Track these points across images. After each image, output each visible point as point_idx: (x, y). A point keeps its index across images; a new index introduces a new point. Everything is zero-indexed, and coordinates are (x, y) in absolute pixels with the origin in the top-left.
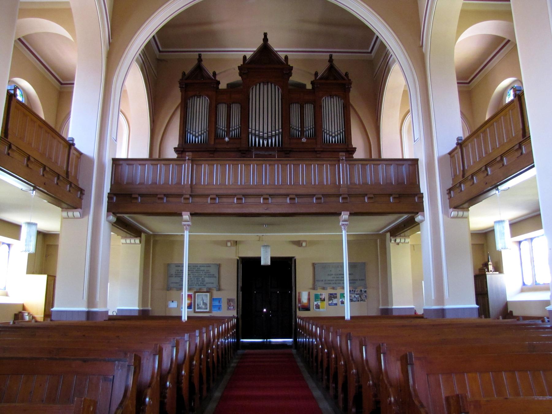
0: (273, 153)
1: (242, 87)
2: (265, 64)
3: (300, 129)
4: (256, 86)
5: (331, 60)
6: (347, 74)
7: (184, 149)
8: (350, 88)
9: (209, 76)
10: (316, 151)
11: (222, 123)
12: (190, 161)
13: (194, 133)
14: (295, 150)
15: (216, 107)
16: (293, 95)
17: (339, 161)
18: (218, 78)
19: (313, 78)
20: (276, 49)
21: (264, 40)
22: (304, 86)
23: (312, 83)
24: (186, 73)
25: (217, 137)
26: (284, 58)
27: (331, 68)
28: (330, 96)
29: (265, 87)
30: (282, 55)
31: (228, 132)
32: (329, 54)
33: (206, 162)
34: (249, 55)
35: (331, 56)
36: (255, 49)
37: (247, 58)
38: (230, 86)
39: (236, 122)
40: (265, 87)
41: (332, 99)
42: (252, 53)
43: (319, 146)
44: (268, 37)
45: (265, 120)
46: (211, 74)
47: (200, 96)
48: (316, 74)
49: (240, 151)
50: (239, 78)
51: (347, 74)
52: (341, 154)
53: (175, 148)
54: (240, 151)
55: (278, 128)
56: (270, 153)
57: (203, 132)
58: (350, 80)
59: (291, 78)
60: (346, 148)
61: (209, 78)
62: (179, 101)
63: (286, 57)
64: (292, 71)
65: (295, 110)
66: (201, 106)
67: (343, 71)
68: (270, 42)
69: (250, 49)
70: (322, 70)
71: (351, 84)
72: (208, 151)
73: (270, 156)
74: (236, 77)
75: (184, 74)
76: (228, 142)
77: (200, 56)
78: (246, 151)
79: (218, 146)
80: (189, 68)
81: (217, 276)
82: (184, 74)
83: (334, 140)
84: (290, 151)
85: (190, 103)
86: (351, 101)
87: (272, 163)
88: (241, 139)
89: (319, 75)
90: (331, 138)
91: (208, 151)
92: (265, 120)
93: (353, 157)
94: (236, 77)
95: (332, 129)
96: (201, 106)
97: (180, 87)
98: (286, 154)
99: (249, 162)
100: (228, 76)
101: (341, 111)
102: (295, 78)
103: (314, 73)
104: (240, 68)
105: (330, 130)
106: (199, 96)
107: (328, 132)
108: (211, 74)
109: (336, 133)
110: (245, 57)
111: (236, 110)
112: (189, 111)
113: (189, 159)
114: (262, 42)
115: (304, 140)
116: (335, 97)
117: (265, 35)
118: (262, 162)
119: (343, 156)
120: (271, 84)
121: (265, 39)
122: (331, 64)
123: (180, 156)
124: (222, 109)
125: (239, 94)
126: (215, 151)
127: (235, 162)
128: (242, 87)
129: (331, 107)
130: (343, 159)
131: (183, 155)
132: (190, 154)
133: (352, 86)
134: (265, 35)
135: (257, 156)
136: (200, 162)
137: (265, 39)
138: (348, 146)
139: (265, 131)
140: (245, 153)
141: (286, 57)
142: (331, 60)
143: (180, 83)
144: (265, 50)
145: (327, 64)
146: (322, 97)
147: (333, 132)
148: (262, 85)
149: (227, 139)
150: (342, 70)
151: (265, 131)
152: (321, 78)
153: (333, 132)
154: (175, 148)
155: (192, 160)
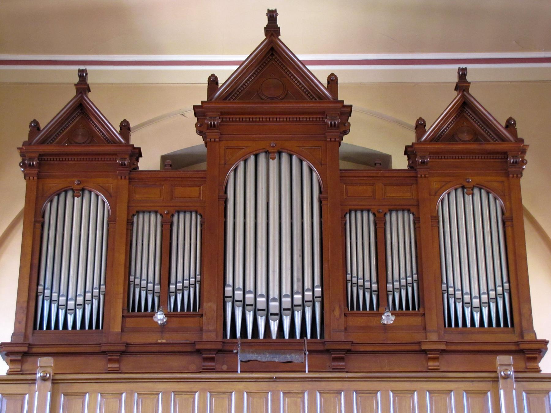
0: (296, 358)
1: (203, 166)
2: (271, 100)
3: (375, 287)
4: (245, 161)
5: (462, 84)
6: (510, 125)
7: (30, 346)
8: (524, 162)
9: (108, 131)
10: (425, 352)
11: (146, 271)
12: (49, 384)
13: (62, 300)
14: (362, 348)
15: (130, 223)
16: (353, 189)
17: (496, 380)
18: (135, 140)
19: (411, 138)
20: (302, 57)
21: (267, 30)
22: (386, 159)
23: (409, 152)
24: (42, 126)
25: (133, 310)
26: (325, 81)
27: (465, 107)
28: (463, 188)
29: (273, 164)
30: (320, 74)
31: (164, 295)
32: (456, 67)
33: (96, 386)
34: (224, 74)
35: (462, 74)
36: (243, 58)
37: (221, 82)
38: (171, 162)
39: (186, 267)
40: (273, 164)
41: (469, 198)
42: (235, 67)
43: (434, 337)
44: (279, 23)
45: (272, 260)
46: (115, 128)
47: (83, 190)
48: (420, 126)
49: (199, 352)
50: (198, 141)
51: (510, 125)
52: (500, 359)
53: (195, 107)
54: (199, 352)
55: (311, 276)
56: (288, 358)
57: (88, 296)
58: (522, 140)
59: (346, 139)
60: (517, 343)
61: (112, 141)
62: (20, 205)
63: (333, 80)
64: (350, 119)
65: (360, 231)
66: (83, 218)
67: (499, 118)
68: (285, 37)
69: (231, 52)
70: (437, 110)
71: (524, 152)
72: (104, 353)
73: (289, 367)
74: (186, 138)
75: (35, 127)
76: (163, 325)
77: (83, 75)
78: (219, 351)
79: (136, 339)
80: (48, 114)
81: (254, 292)
82: (35, 127)
83: (477, 317)
84: (349, 351)
85: (51, 211)
86: (525, 203)
87: (295, 387)
88: (202, 315)
89: (430, 129)
90: (468, 311)
91: (104, 353)
92: (272, 260)
93: (538, 370)
94: (186, 138)
95: (470, 281)
96: (83, 218)
97: (23, 165)
98: (335, 359)
99: (224, 387)
100: (166, 134)
101: (497, 230)
102: (359, 138)
103: (413, 124)
104: (199, 111)
105: (466, 289)
106: (80, 192)
107: (459, 294)
108: (115, 128)
109: (484, 298)
110: (213, 81)
111: (187, 229)
112: (50, 233)
113: (44, 379)
114: (262, 37)
115: (388, 318)
116: (476, 191)
117: (272, 16)
118: (263, 386)
119: (505, 364)
120: (291, 156)
121: (272, 29)
122: (463, 96)
123: (17, 367)
124: (148, 228)
125: (195, 188)
126: (123, 353)
127: (183, 387)
128: (203, 166)
129: (467, 218)
130: (507, 377)
131: (27, 366)
132: (49, 361)
133: (527, 157)
134: (272, 16)
135: (250, 367)
136: (77, 388)
137: (272, 29)
138: (522, 335)
139: (274, 293)
140: (212, 359)
141: (333, 80)
142: (462, 84)
143: (22, 155)
144: (272, 56)
145: (451, 98)
146: (437, 193)
147: (475, 293)
148: (262, 158)
149: (160, 317)
150: (497, 112)
151: (274, 293)
152: (435, 138)
153: (475, 293)
154: (195, 107)
155: (55, 382)
